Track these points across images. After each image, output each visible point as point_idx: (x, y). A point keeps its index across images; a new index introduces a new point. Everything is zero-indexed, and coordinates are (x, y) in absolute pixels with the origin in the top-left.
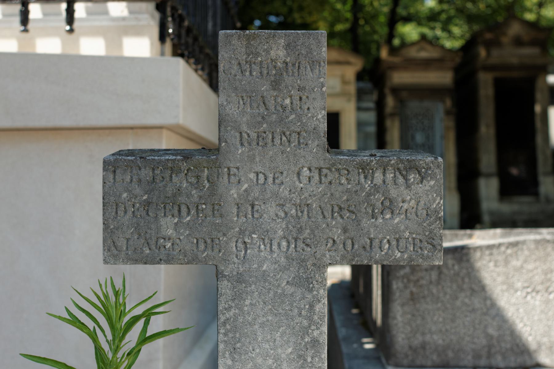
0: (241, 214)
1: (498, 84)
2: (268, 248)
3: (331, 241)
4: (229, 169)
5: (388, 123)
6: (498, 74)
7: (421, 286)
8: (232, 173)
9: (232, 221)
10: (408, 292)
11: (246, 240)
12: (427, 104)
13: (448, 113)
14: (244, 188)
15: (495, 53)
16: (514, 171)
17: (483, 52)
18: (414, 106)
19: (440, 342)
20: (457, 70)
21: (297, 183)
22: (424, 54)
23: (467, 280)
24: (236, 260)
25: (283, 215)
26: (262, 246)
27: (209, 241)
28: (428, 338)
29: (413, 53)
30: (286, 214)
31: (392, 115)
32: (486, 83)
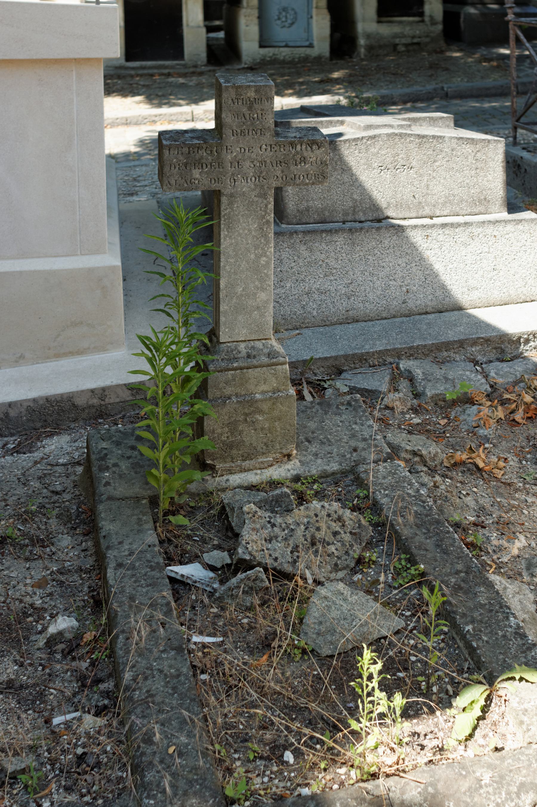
28: (311, 203)
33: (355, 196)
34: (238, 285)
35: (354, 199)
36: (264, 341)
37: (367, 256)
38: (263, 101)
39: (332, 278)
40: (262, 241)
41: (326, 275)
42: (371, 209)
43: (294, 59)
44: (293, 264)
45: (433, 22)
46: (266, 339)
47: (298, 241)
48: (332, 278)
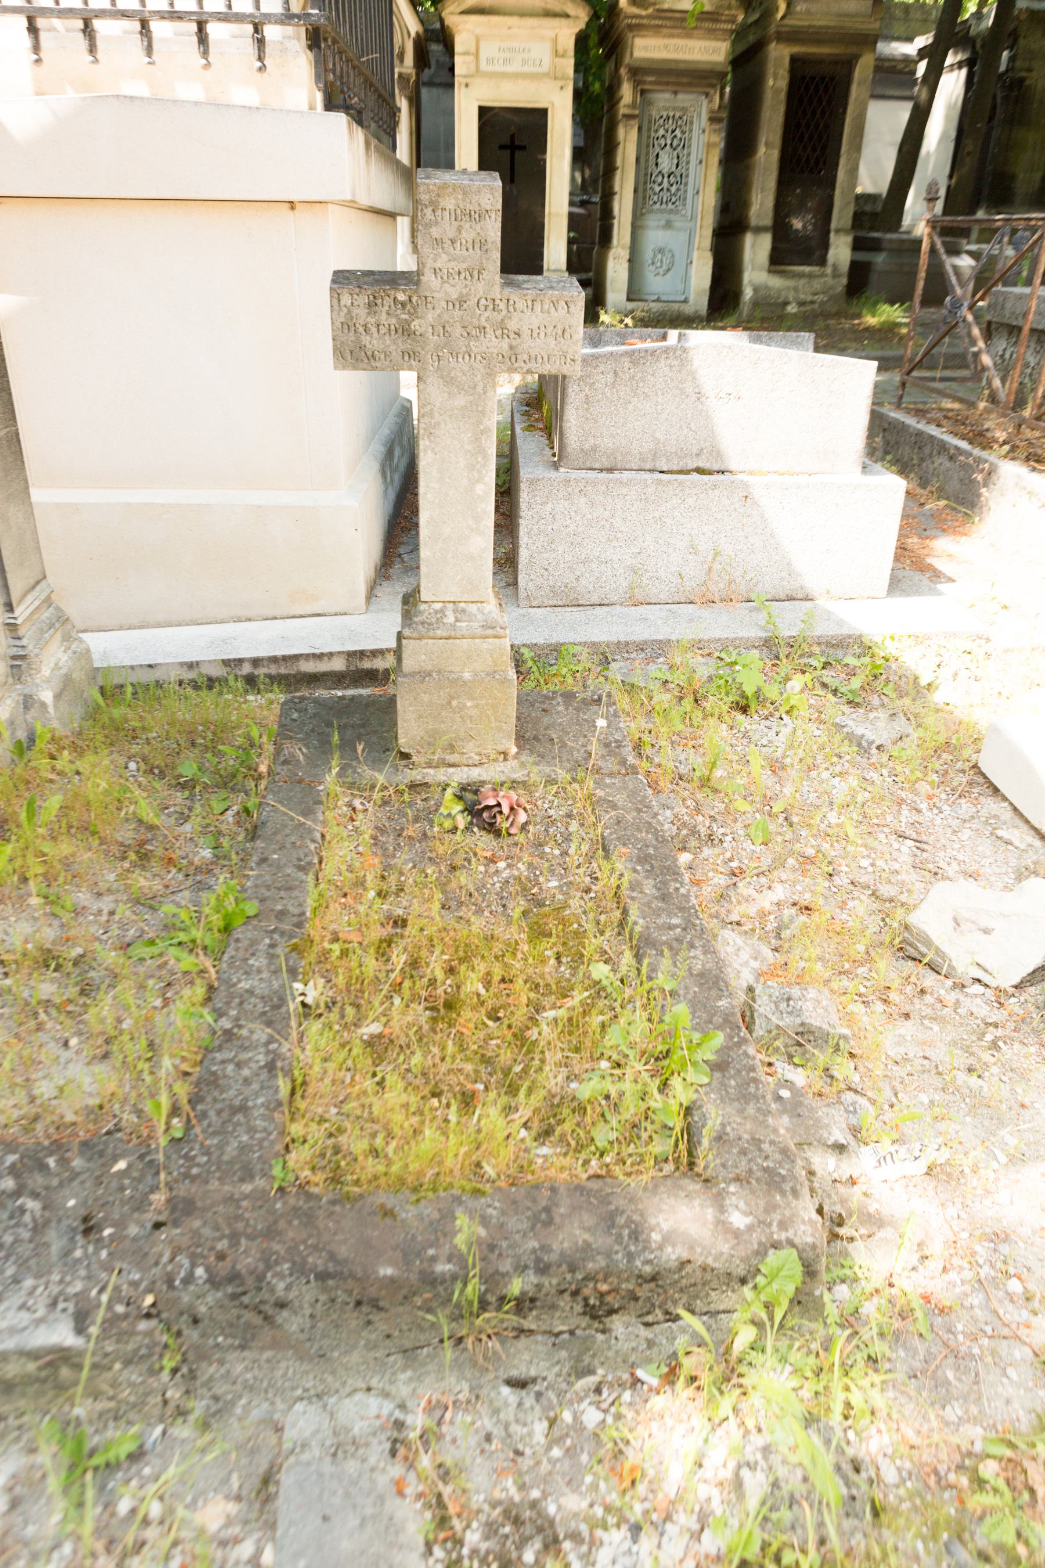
6: (797, 49)
12: (684, 99)
13: (712, 120)
16: (797, 224)
18: (663, 100)
20: (739, 34)
33: (658, 435)
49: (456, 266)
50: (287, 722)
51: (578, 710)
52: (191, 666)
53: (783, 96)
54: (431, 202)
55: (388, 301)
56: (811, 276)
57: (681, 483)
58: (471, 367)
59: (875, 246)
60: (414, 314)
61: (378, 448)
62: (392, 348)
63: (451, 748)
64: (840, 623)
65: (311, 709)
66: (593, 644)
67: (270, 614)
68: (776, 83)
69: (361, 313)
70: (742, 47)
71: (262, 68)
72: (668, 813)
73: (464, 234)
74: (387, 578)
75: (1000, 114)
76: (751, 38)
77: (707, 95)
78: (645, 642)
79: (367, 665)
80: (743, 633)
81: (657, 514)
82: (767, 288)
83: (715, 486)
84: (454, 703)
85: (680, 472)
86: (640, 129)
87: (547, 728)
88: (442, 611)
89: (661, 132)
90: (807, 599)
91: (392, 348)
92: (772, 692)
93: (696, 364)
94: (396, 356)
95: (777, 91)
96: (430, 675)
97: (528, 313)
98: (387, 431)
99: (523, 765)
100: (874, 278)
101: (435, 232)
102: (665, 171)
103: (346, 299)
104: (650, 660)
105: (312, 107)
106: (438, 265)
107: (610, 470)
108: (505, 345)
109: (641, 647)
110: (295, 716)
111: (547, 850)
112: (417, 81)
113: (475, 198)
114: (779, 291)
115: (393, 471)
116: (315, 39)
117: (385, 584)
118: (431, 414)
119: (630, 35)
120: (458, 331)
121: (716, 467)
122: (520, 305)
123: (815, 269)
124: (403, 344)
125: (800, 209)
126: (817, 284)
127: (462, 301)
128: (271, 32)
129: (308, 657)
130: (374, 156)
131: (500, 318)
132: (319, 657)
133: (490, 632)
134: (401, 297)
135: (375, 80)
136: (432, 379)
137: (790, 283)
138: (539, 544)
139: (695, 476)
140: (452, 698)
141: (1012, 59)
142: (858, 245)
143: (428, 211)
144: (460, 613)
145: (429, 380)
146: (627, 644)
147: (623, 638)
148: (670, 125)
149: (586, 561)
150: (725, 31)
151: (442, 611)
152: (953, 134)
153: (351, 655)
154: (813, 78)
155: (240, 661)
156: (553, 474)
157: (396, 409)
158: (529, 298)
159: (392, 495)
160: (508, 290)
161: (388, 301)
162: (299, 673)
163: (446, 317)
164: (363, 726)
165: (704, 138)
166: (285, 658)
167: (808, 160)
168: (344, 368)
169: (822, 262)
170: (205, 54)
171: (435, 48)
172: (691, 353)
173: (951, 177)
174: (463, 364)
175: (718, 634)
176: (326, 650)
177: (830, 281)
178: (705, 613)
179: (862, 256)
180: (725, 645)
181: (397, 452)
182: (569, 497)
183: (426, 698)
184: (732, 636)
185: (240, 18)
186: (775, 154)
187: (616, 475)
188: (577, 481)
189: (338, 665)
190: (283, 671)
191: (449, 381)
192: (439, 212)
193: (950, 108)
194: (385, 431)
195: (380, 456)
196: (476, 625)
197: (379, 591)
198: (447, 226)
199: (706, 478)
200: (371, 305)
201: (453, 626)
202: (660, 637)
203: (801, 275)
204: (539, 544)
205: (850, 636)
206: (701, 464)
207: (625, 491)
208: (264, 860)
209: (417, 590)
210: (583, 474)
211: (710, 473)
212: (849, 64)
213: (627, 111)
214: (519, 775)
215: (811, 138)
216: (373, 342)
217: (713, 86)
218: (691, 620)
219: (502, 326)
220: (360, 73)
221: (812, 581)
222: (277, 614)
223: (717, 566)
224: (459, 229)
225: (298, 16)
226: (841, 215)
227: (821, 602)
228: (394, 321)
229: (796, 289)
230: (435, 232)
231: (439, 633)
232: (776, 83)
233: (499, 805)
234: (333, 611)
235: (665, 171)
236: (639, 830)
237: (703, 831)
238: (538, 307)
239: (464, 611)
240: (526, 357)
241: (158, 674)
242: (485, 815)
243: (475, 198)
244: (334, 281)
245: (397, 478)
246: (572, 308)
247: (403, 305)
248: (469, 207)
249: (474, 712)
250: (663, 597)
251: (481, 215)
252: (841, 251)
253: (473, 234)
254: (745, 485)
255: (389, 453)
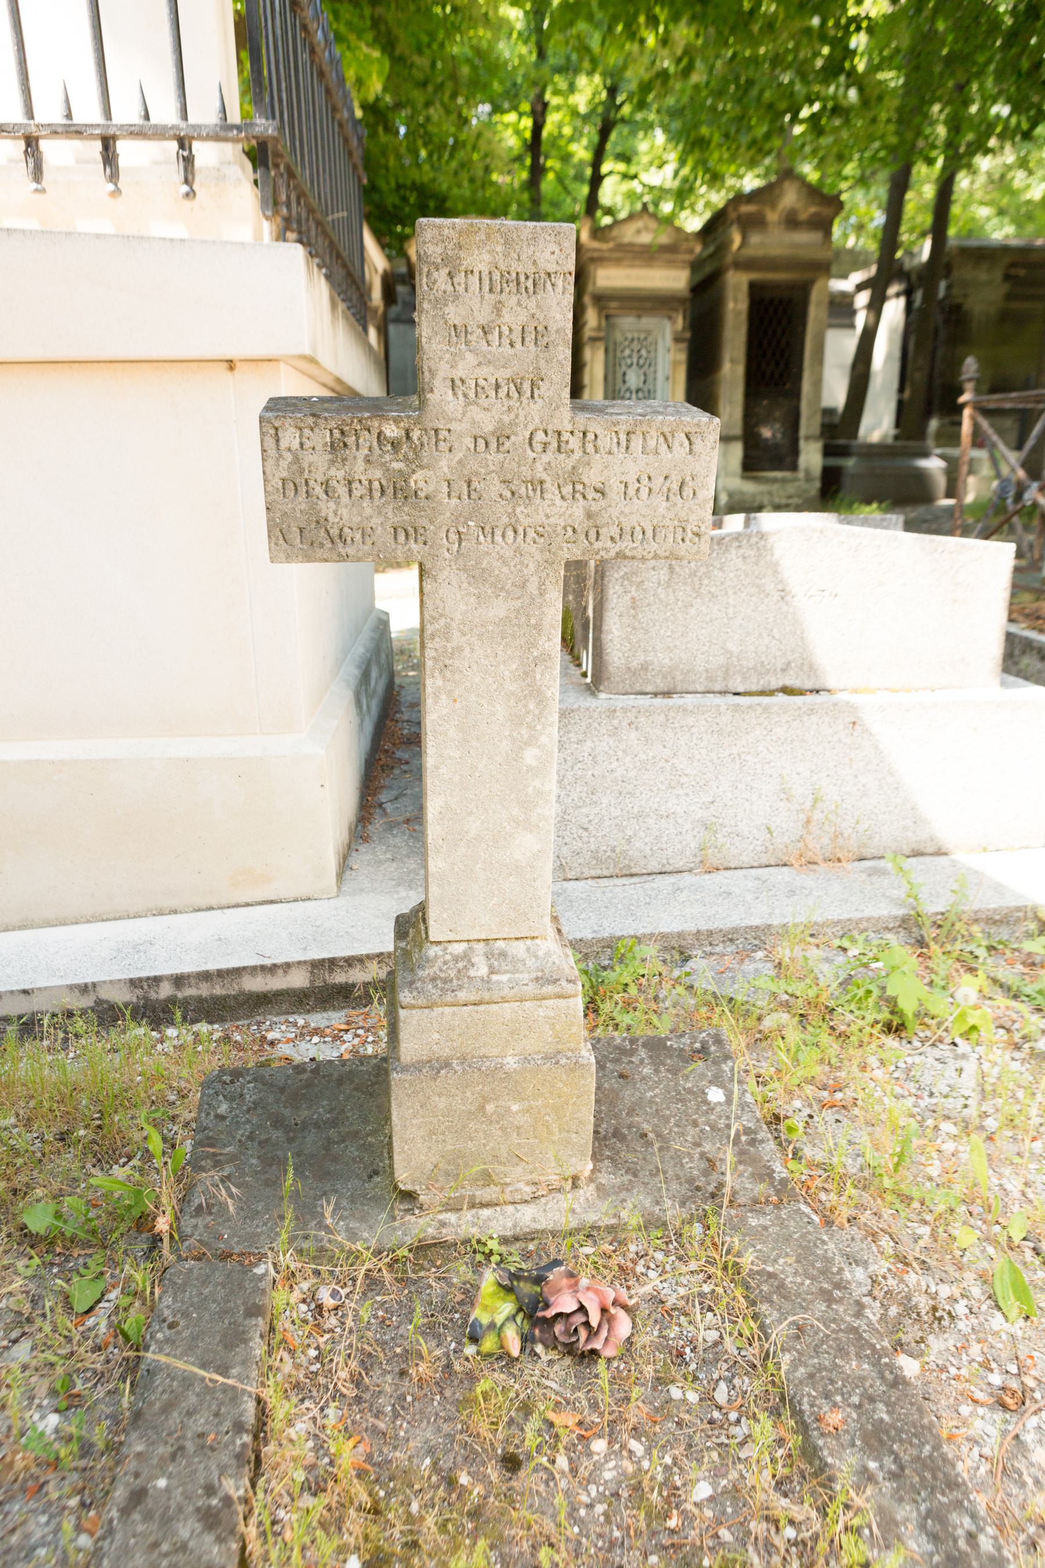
0: (453, 494)
1: (755, 290)
2: (489, 539)
3: (570, 530)
4: (436, 431)
5: (587, 353)
6: (755, 276)
7: (645, 590)
8: (441, 437)
9: (441, 503)
10: (627, 598)
11: (461, 529)
12: (648, 322)
13: (677, 340)
14: (457, 459)
15: (755, 239)
16: (766, 433)
17: (737, 239)
18: (627, 323)
19: (667, 661)
20: (695, 266)
21: (529, 451)
22: (646, 238)
23: (705, 582)
24: (447, 555)
25: (509, 495)
26: (481, 537)
27: (411, 531)
28: (651, 657)
29: (629, 234)
30: (513, 493)
31: (594, 339)
32: (736, 287)
33: (731, 646)
34: (471, 813)
35: (727, 651)
36: (529, 942)
37: (743, 756)
38: (540, 286)
39: (681, 792)
40: (531, 706)
41: (671, 787)
42: (756, 670)
43: (646, 135)
44: (615, 764)
45: (809, 478)
46: (533, 938)
47: (625, 724)
48: (681, 792)
49: (490, 374)
50: (209, 1121)
51: (674, 1071)
52: (84, 989)
53: (744, 317)
54: (446, 260)
55: (367, 440)
56: (783, 481)
57: (766, 709)
58: (518, 551)
59: (844, 452)
60: (415, 461)
61: (351, 672)
62: (376, 521)
63: (487, 1178)
64: (999, 889)
65: (251, 1093)
66: (664, 936)
67: (204, 904)
68: (736, 307)
69: (318, 461)
70: (700, 277)
71: (191, 194)
72: (860, 1273)
73: (507, 317)
74: (366, 839)
75: (942, 334)
76: (708, 269)
77: (670, 318)
78: (736, 930)
79: (339, 978)
80: (870, 911)
81: (735, 751)
82: (741, 493)
83: (812, 711)
84: (490, 1108)
85: (762, 693)
86: (606, 351)
87: (631, 1112)
88: (466, 957)
89: (627, 352)
90: (939, 853)
91: (376, 521)
92: (938, 1004)
93: (778, 553)
94: (383, 536)
95: (738, 314)
96: (447, 1064)
97: (620, 454)
98: (362, 650)
99: (602, 1191)
100: (846, 481)
101: (454, 314)
102: (633, 388)
103: (290, 438)
104: (744, 956)
105: (258, 236)
106: (459, 373)
107: (667, 694)
108: (578, 510)
109: (729, 937)
110: (223, 1108)
111: (676, 1393)
112: (385, 313)
113: (527, 252)
114: (754, 496)
115: (370, 697)
116: (259, 155)
117: (363, 848)
118: (447, 635)
119: (592, 267)
120: (494, 487)
121: (809, 685)
122: (606, 441)
123: (787, 474)
124: (394, 514)
125: (766, 421)
126: (791, 489)
127: (502, 436)
128: (204, 153)
129: (253, 970)
130: (341, 323)
131: (570, 463)
132: (271, 969)
133: (550, 989)
134: (391, 431)
135: (345, 254)
136: (447, 573)
137: (763, 488)
138: (575, 796)
139: (781, 698)
140: (486, 1100)
141: (949, 287)
142: (828, 451)
143: (441, 276)
144: (497, 958)
145: (442, 576)
146: (710, 933)
147: (704, 927)
148: (636, 346)
149: (638, 817)
150: (684, 262)
151: (466, 956)
152: (897, 354)
153: (316, 965)
154: (771, 302)
155: (157, 980)
156: (589, 702)
157: (370, 624)
158: (622, 429)
159: (369, 727)
160: (582, 418)
161: (367, 440)
162: (242, 993)
163: (473, 465)
164: (334, 1123)
165: (671, 357)
166: (221, 974)
167: (772, 374)
168: (288, 558)
169: (794, 467)
170: (114, 176)
171: (401, 289)
172: (771, 540)
173: (901, 389)
174: (504, 546)
175: (835, 913)
176: (280, 960)
177: (803, 484)
178: (806, 880)
179: (833, 462)
180: (847, 929)
181: (374, 673)
182: (614, 732)
183: (442, 1103)
184: (856, 915)
185: (159, 133)
186: (740, 370)
187: (675, 700)
188: (625, 710)
189: (299, 980)
190: (218, 991)
191: (478, 576)
192: (460, 278)
193: (892, 331)
194: (360, 649)
195: (353, 682)
196: (525, 977)
197: (355, 861)
198: (475, 303)
199: (798, 700)
200: (337, 447)
201: (487, 981)
202: (755, 922)
203: (775, 480)
204: (575, 796)
205: (1018, 909)
206: (789, 681)
207: (690, 720)
208: (138, 1496)
209: (420, 912)
210: (631, 700)
211: (801, 693)
212: (804, 289)
213: (593, 334)
214: (599, 1215)
215: (773, 354)
216: (340, 512)
217: (676, 310)
218: (792, 893)
219: (574, 478)
220: (326, 234)
221: (944, 827)
222: (214, 903)
223: (817, 816)
224: (498, 308)
225: (238, 128)
226: (809, 424)
227: (959, 856)
228: (378, 473)
229: (770, 493)
230: (454, 314)
231: (462, 995)
232: (736, 307)
233: (582, 1309)
234: (292, 895)
235: (633, 388)
236: (842, 1352)
237: (923, 1304)
238: (637, 443)
239: (503, 954)
240: (614, 531)
241: (35, 1004)
242: (558, 1328)
243: (527, 252)
244: (267, 409)
245: (375, 705)
246: (698, 446)
247: (395, 445)
248: (516, 267)
249: (522, 1120)
250: (746, 859)
251: (536, 283)
252: (811, 457)
253: (523, 317)
254: (853, 708)
255: (365, 676)
